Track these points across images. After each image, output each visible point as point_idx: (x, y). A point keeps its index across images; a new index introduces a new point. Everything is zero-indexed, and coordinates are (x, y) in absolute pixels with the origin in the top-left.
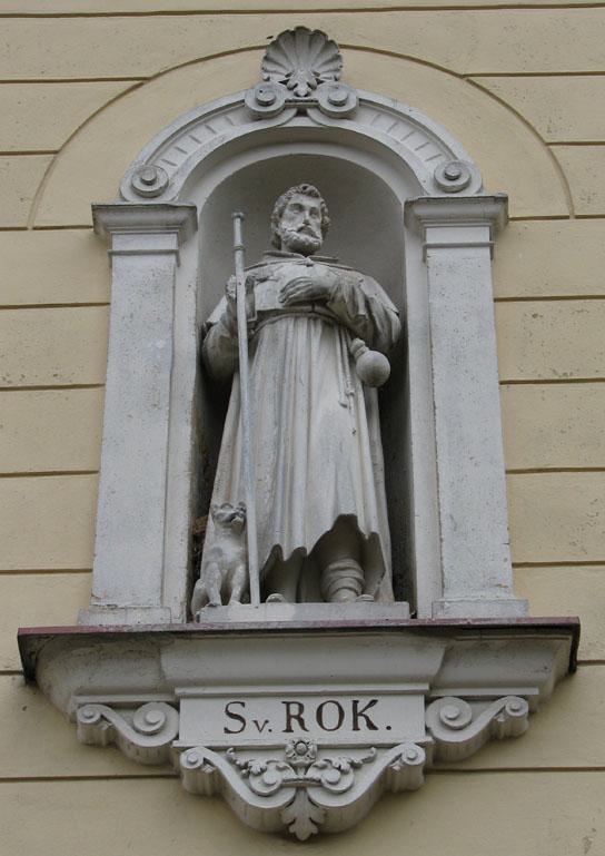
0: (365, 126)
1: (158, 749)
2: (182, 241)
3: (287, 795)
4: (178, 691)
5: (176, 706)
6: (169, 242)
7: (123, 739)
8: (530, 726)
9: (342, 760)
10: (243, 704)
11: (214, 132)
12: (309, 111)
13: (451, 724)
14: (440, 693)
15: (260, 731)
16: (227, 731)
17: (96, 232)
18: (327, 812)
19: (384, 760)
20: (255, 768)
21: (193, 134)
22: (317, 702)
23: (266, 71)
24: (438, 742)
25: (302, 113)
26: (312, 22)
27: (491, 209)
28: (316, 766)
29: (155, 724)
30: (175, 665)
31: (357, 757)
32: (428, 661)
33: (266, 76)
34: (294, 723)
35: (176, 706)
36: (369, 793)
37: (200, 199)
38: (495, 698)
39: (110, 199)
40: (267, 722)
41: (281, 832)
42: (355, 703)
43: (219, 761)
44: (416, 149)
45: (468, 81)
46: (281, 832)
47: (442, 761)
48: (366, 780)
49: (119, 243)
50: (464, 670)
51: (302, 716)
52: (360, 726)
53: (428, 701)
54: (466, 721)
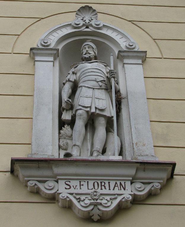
0: (104, 31)
1: (52, 194)
2: (55, 59)
4: (58, 177)
5: (57, 182)
6: (52, 59)
7: (41, 190)
8: (160, 191)
9: (108, 198)
10: (70, 182)
11: (58, 34)
12: (89, 27)
13: (140, 189)
14: (134, 181)
15: (75, 189)
16: (66, 188)
17: (30, 55)
18: (103, 211)
19: (119, 198)
20: (82, 199)
22: (93, 181)
23: (77, 17)
24: (134, 194)
25: (87, 27)
26: (90, 5)
27: (142, 55)
28: (100, 199)
29: (52, 186)
30: (57, 170)
31: (113, 197)
32: (132, 172)
33: (77, 18)
34: (103, 187)
35: (57, 182)
36: (115, 208)
37: (60, 47)
38: (150, 183)
39: (35, 46)
40: (76, 186)
41: (88, 218)
43: (71, 197)
44: (120, 39)
45: (132, 23)
46: (88, 218)
47: (136, 201)
48: (115, 203)
49: (37, 58)
50: (141, 174)
51: (105, 185)
53: (132, 183)
54: (143, 188)
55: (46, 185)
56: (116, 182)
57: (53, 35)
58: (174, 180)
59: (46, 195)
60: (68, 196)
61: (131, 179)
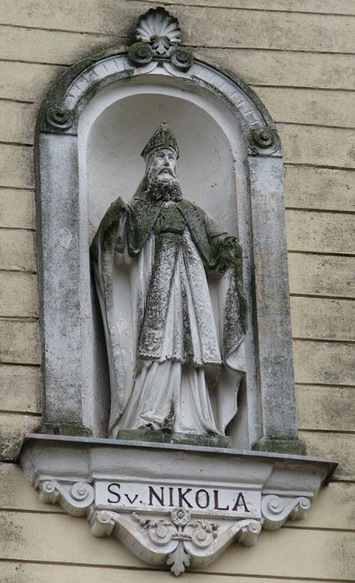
3: (174, 545)
5: (92, 484)
7: (65, 501)
13: (272, 509)
16: (109, 501)
21: (104, 64)
24: (266, 520)
35: (92, 484)
42: (180, 490)
52: (153, 503)
55: (75, 488)
56: (240, 495)
57: (105, 67)
58: (327, 488)
59: (141, 554)
60: (57, 488)
61: (260, 486)
